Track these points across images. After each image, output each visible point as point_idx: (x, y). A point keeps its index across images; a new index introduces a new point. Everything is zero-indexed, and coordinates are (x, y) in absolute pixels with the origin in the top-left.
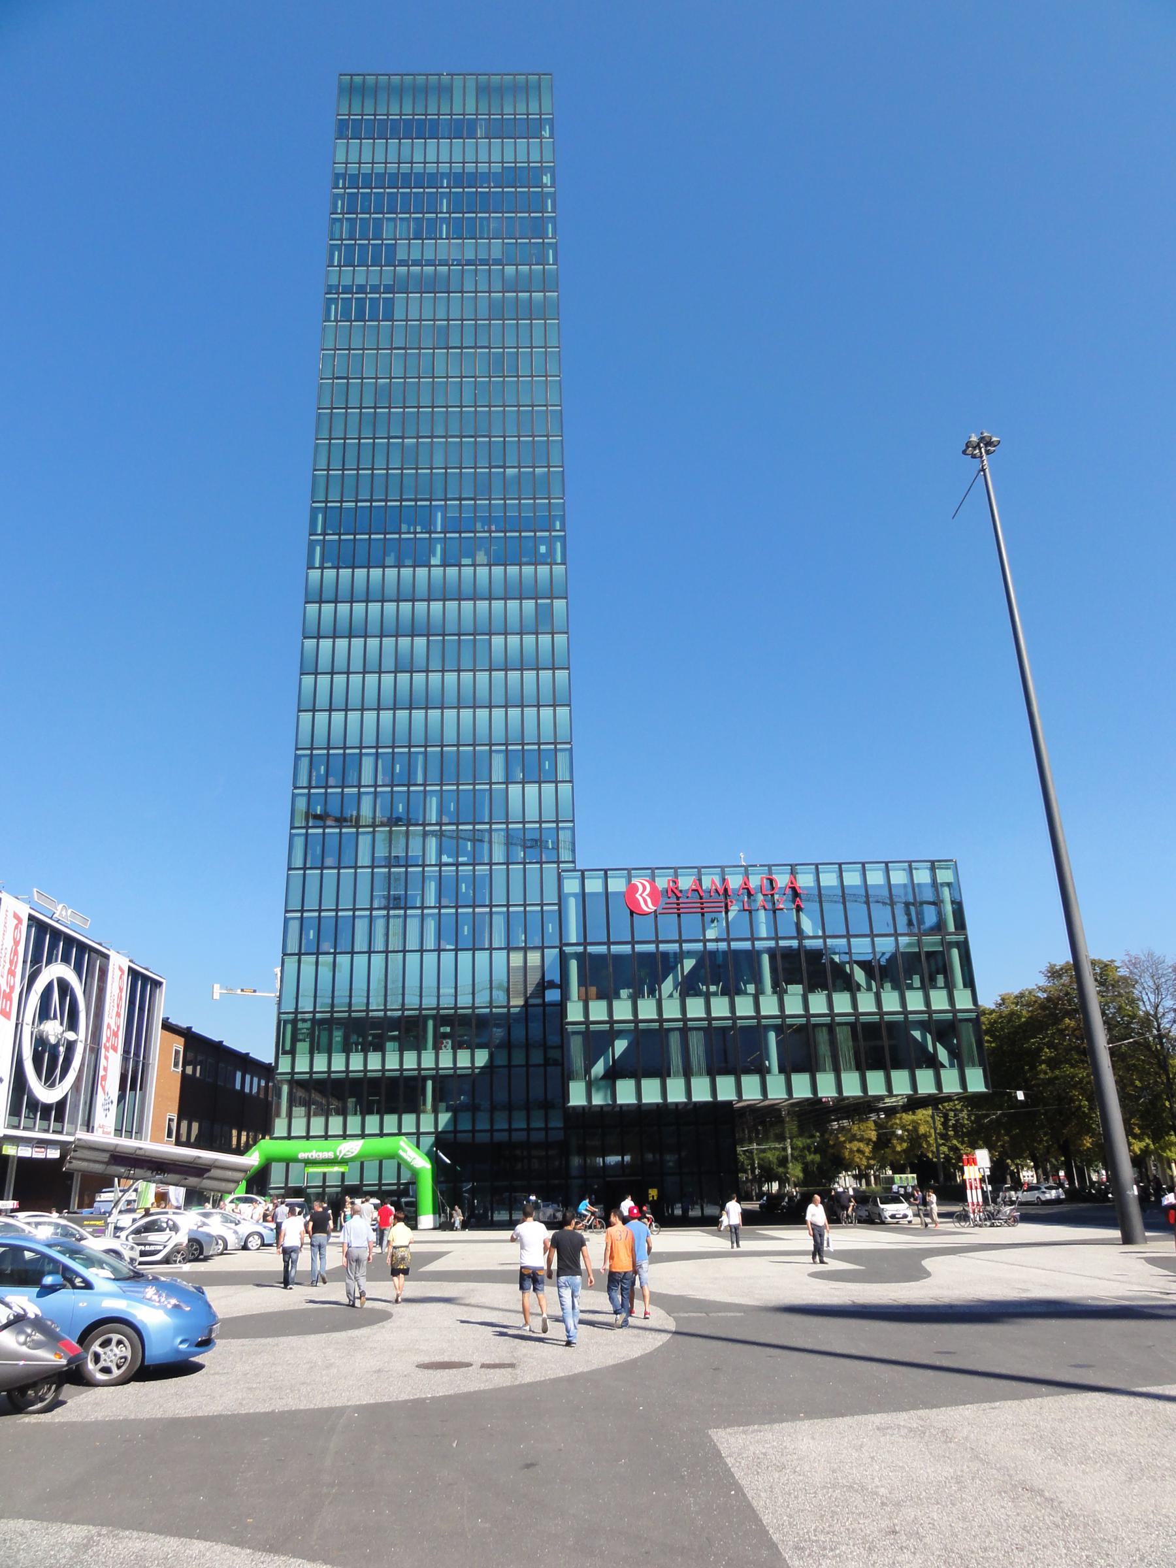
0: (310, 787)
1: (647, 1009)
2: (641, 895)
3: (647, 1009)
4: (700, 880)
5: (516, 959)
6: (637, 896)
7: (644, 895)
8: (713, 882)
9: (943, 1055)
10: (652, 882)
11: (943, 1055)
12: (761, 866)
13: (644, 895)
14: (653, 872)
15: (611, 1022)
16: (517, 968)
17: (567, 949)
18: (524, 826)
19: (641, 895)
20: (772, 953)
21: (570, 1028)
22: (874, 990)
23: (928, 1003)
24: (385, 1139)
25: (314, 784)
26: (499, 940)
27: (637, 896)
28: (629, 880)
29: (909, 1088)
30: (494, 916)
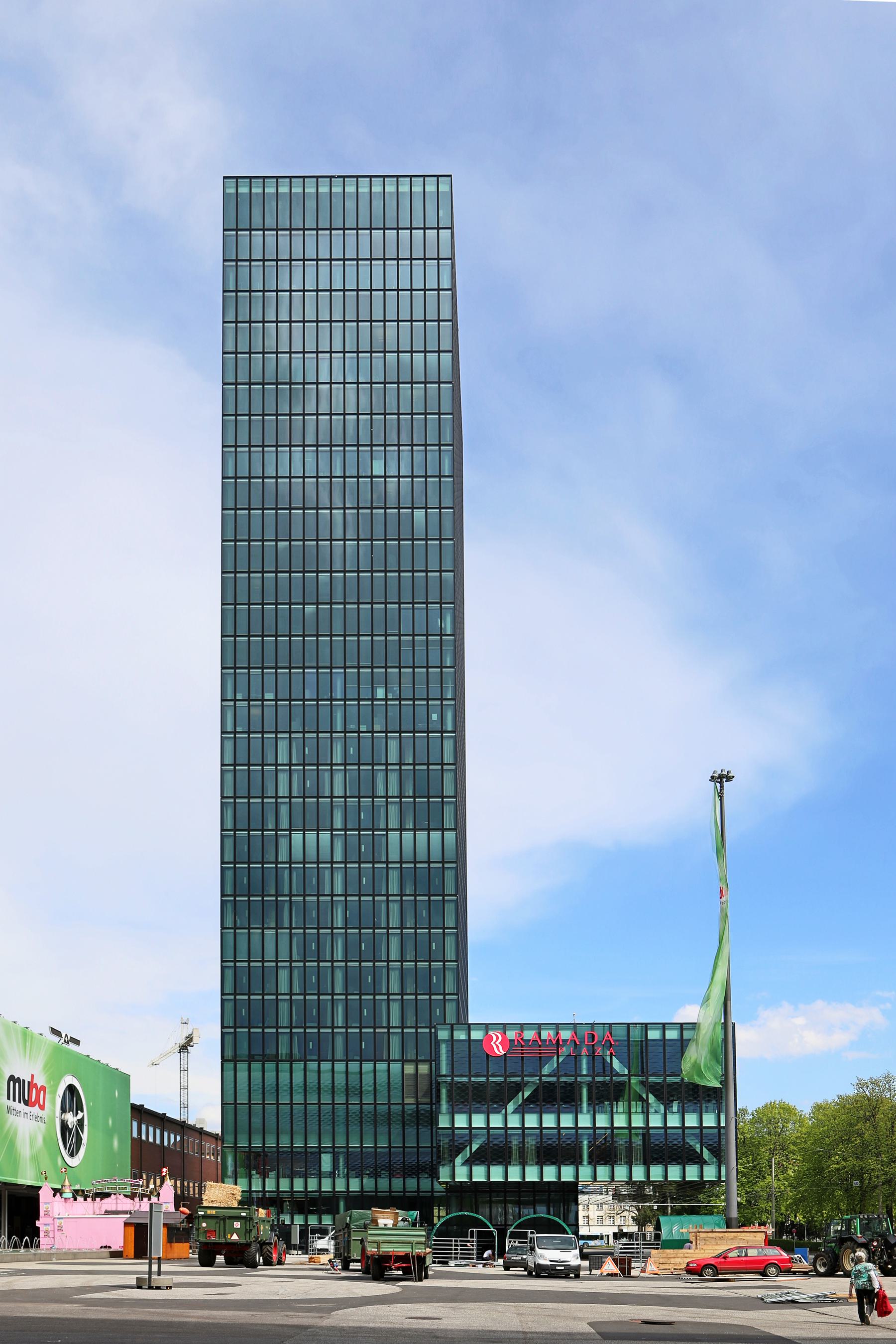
0: (291, 1027)
1: (496, 1121)
2: (494, 1043)
3: (496, 1121)
4: (540, 1034)
5: (409, 1069)
6: (492, 1043)
7: (497, 1043)
8: (549, 1034)
9: (706, 1154)
10: (504, 1034)
11: (706, 1154)
12: (586, 1024)
13: (497, 1043)
14: (504, 1027)
15: (470, 1128)
16: (410, 1075)
17: (440, 1079)
18: (416, 931)
19: (494, 1043)
20: (590, 1086)
21: (440, 1132)
22: (663, 1112)
23: (470, 1175)
24: (603, 1227)
25: (294, 1025)
26: (395, 1053)
27: (492, 1043)
28: (487, 1033)
29: (643, 1177)
30: (390, 871)
